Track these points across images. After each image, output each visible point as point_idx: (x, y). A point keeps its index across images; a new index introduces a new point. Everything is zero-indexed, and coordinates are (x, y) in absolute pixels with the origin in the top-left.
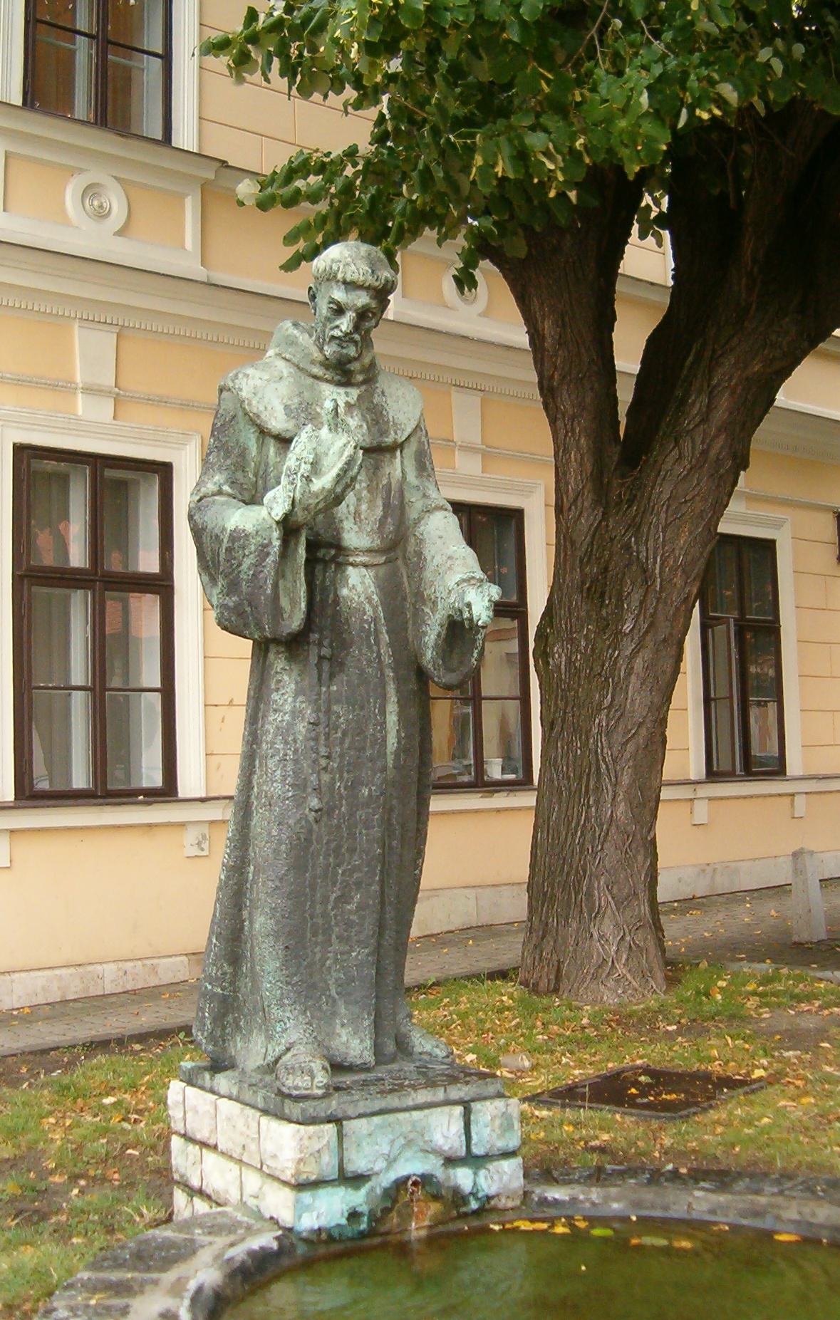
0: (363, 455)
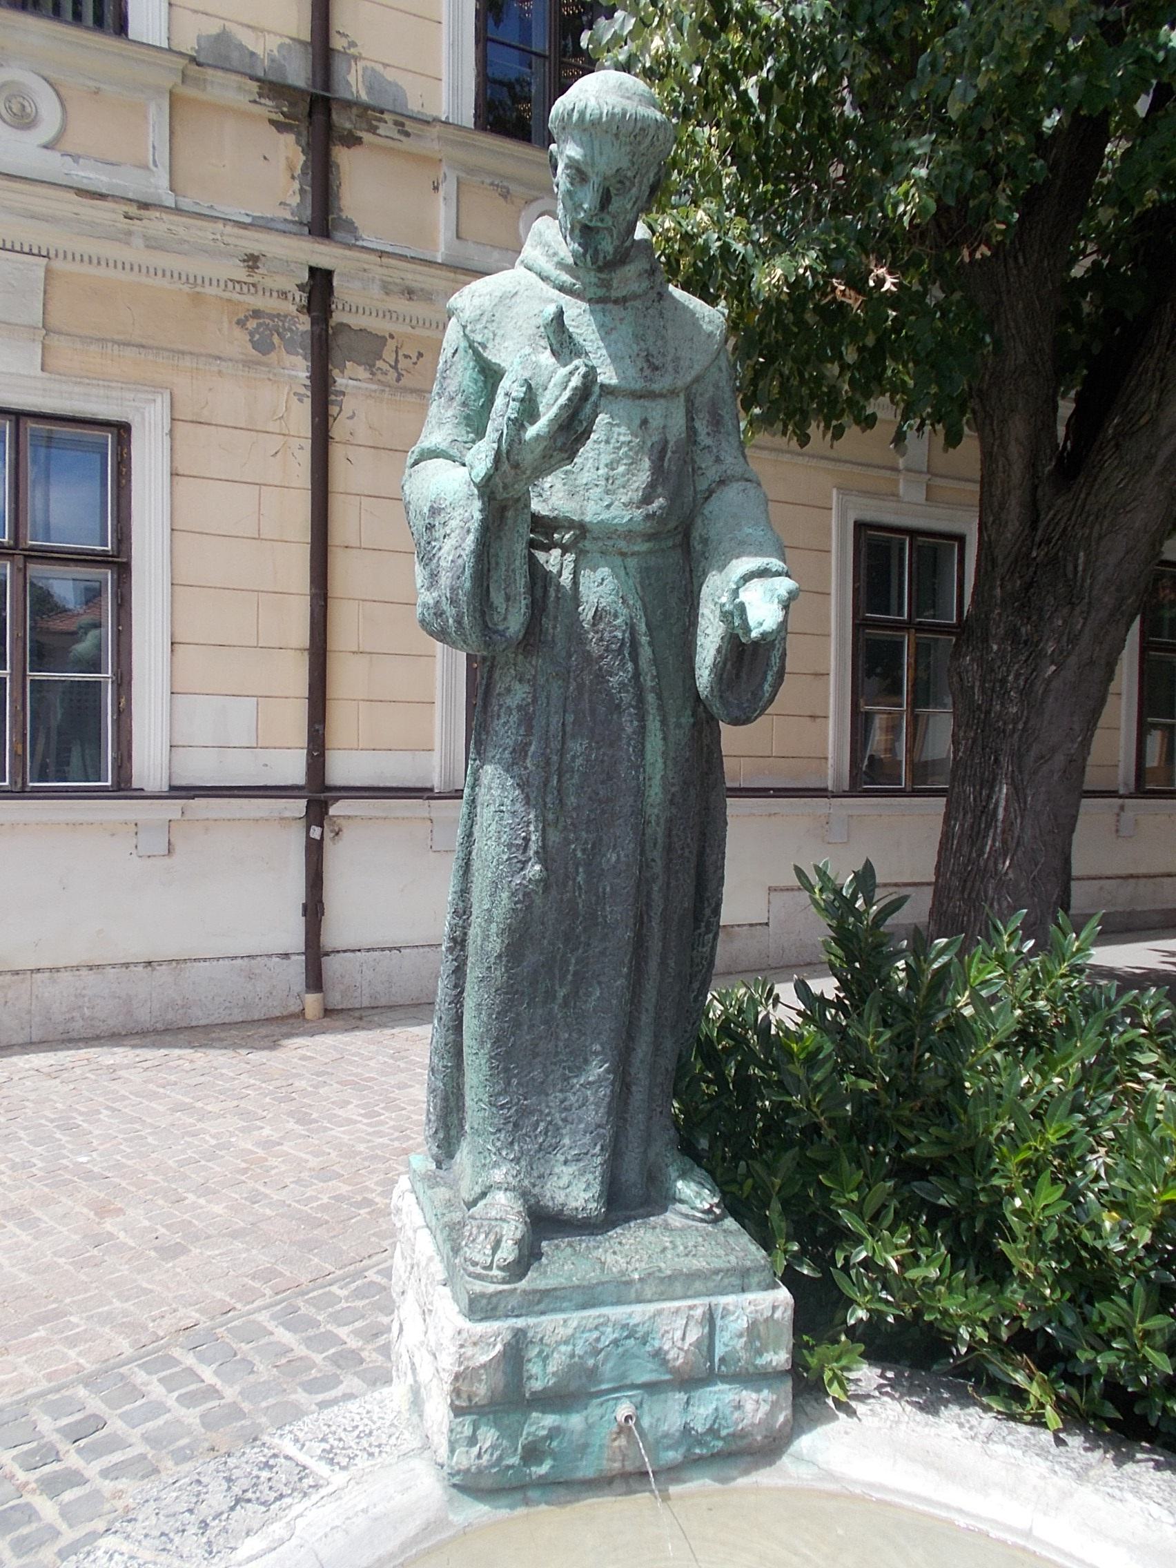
0: (838, 494)
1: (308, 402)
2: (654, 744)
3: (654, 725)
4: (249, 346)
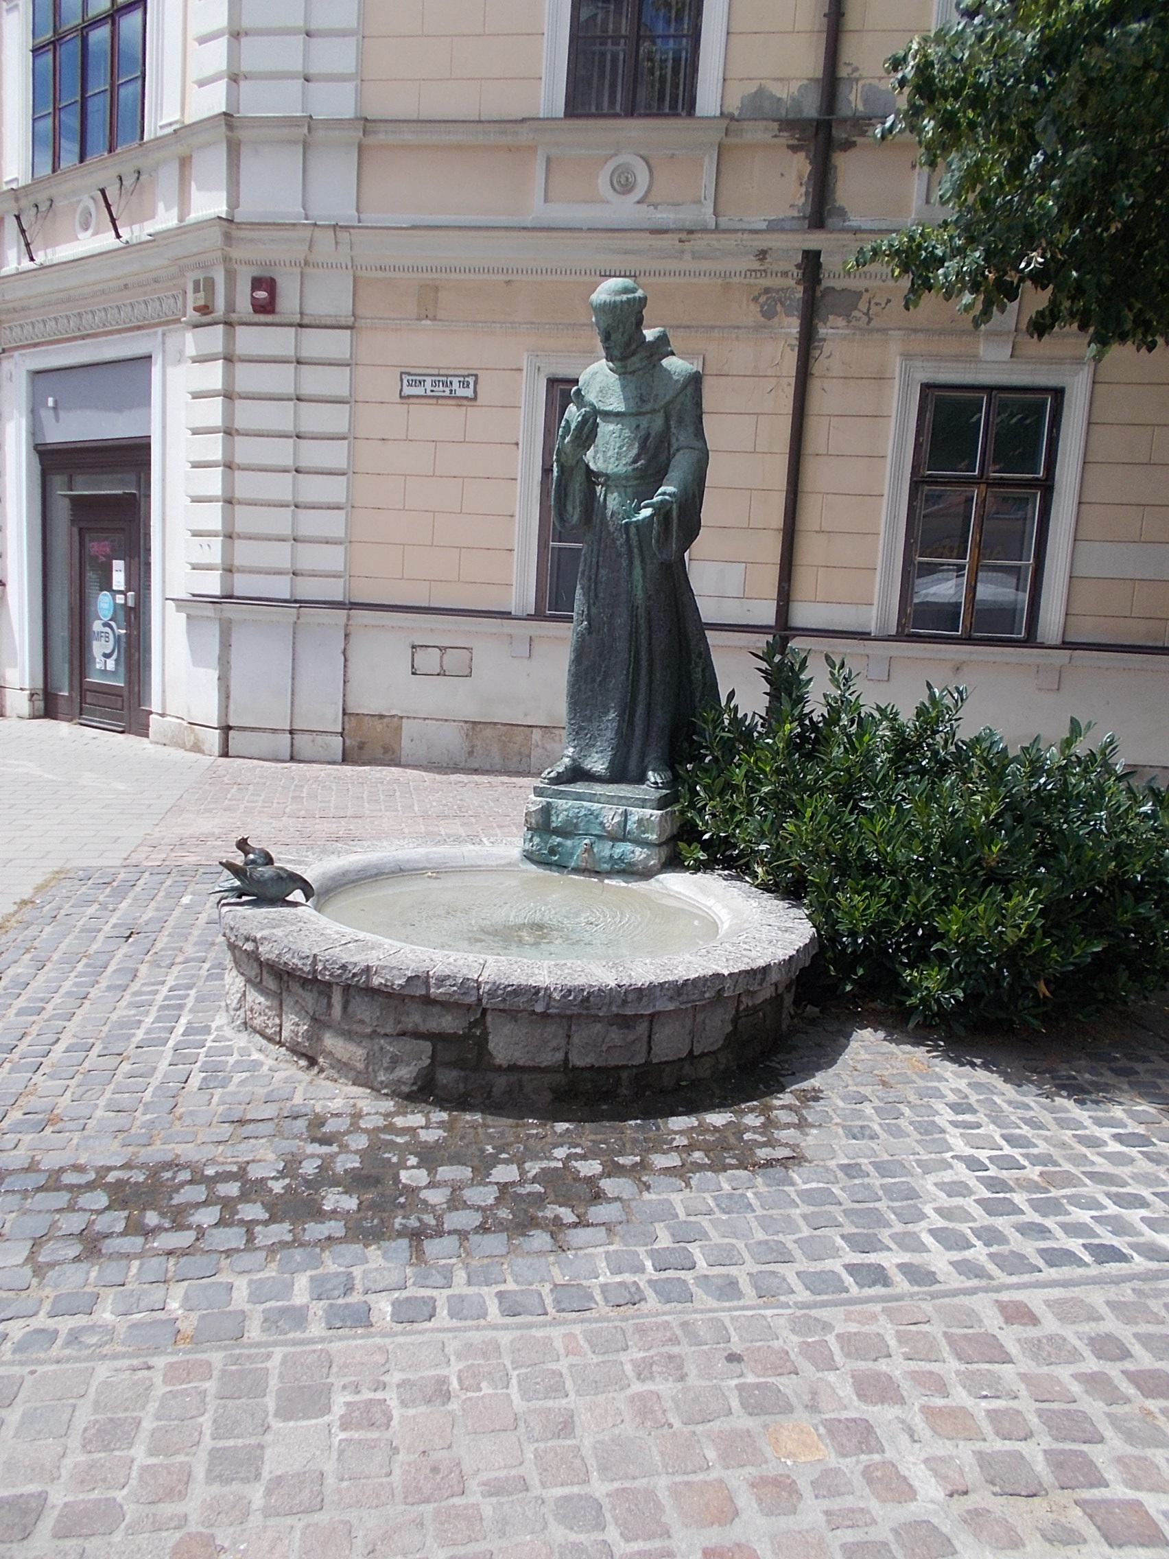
1: (796, 349)
2: (638, 571)
3: (637, 562)
4: (759, 315)
